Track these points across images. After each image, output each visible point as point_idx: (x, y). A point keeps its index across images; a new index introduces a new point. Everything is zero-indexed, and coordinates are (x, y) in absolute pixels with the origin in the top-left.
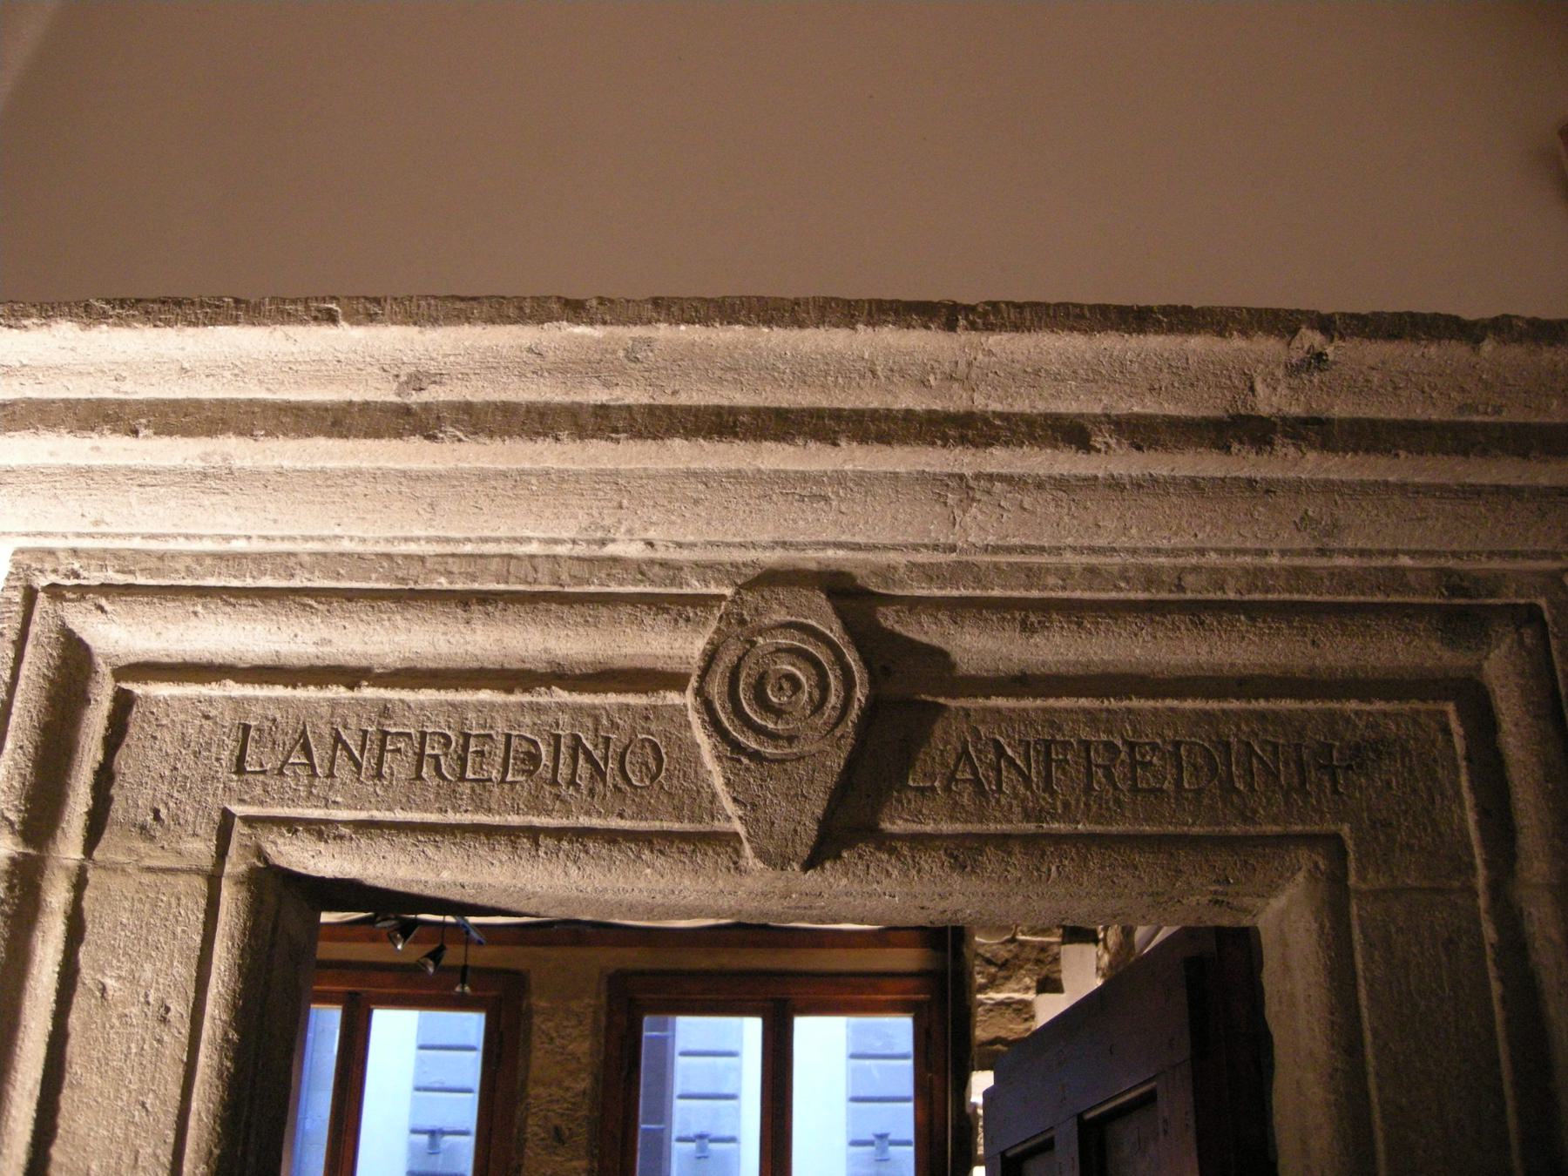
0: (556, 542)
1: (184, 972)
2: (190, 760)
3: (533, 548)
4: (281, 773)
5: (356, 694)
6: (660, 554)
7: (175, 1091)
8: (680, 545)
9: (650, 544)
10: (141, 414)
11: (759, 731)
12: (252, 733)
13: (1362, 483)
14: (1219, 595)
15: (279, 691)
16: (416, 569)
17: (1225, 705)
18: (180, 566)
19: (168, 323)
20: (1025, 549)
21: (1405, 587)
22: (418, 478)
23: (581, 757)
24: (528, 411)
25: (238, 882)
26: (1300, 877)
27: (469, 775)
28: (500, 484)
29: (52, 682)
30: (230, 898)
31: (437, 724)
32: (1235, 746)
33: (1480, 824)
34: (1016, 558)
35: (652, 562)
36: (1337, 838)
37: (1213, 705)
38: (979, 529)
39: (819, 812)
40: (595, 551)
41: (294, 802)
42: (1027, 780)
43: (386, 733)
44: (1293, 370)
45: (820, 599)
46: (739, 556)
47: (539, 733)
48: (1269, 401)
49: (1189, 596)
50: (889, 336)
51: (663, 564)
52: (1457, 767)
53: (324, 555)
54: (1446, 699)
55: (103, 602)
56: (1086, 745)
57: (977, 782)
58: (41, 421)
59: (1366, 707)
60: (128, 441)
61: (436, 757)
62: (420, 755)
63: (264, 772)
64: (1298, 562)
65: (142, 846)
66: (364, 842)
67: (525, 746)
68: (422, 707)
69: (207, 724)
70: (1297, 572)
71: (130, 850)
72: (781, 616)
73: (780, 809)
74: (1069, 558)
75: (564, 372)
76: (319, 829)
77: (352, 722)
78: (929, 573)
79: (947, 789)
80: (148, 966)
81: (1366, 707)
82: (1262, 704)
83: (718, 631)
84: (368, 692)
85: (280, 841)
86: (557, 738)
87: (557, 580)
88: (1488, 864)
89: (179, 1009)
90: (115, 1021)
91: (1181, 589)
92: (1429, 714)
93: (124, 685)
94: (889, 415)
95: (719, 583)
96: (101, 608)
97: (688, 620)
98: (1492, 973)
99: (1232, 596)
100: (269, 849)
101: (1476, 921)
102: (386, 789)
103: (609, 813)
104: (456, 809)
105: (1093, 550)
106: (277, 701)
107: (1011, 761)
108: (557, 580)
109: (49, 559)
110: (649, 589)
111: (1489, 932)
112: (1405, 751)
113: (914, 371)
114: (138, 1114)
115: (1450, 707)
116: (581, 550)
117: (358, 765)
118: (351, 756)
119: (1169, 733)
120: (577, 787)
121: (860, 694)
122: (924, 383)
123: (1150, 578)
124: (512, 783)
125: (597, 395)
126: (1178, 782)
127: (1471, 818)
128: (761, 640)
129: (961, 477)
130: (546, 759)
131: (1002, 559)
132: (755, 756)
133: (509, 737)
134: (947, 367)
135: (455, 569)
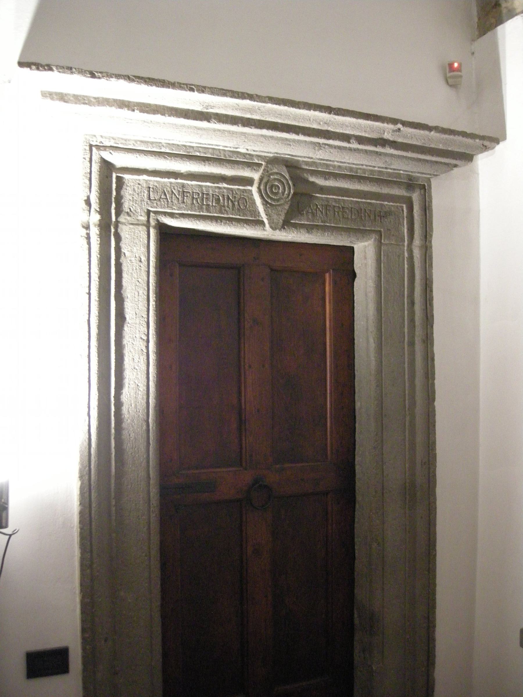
0: (226, 147)
1: (144, 250)
2: (137, 195)
3: (221, 148)
4: (160, 200)
5: (177, 181)
6: (249, 152)
7: (146, 278)
8: (254, 151)
9: (247, 150)
10: (134, 106)
11: (271, 199)
12: (151, 189)
13: (398, 155)
14: (364, 175)
15: (158, 179)
16: (191, 150)
17: (362, 200)
18: (131, 143)
19: (151, 85)
20: (327, 160)
21: (400, 178)
22: (199, 129)
23: (230, 202)
24: (232, 118)
25: (155, 227)
26: (373, 240)
27: (205, 203)
28: (218, 133)
29: (99, 172)
30: (152, 231)
31: (196, 190)
32: (363, 210)
33: (407, 232)
34: (325, 162)
35: (247, 154)
36: (380, 231)
37: (360, 200)
38: (319, 155)
39: (283, 218)
40: (235, 150)
41: (164, 208)
42: (322, 213)
43: (184, 192)
44: (394, 131)
45: (284, 168)
46: (266, 154)
47: (220, 194)
48: (386, 136)
49: (358, 174)
50: (317, 113)
51: (249, 154)
52: (404, 219)
53: (169, 144)
54: (404, 204)
55: (111, 151)
56: (334, 206)
57: (312, 213)
58: (107, 104)
59: (388, 204)
60: (130, 112)
61: (197, 198)
62: (193, 198)
63: (155, 200)
64: (380, 169)
65: (128, 218)
66: (182, 219)
67: (217, 197)
68: (192, 185)
69: (140, 186)
70: (380, 172)
71: (125, 219)
72: (275, 170)
73: (275, 217)
74: (336, 163)
75: (243, 110)
76: (172, 215)
77: (176, 188)
78: (307, 163)
79: (306, 214)
80: (135, 248)
81: (388, 204)
82: (369, 201)
83: (262, 173)
84: (179, 181)
85: (162, 218)
86: (224, 195)
87: (225, 156)
88: (408, 240)
89: (144, 259)
90: (129, 261)
91: (357, 173)
92: (400, 206)
93: (118, 175)
94: (309, 129)
95: (262, 161)
96: (111, 153)
97: (254, 169)
98: (406, 262)
99: (366, 176)
100: (159, 219)
101: (404, 252)
102: (186, 206)
103: (237, 215)
104: (203, 212)
105: (341, 162)
106: (157, 181)
107: (319, 209)
108: (225, 156)
109: (94, 138)
110: (246, 161)
111: (406, 255)
112: (395, 214)
113: (318, 120)
114: (138, 284)
115: (404, 206)
116: (232, 149)
117: (178, 199)
118: (176, 197)
119: (350, 205)
120: (229, 209)
121: (292, 192)
122: (320, 124)
123: (351, 169)
124: (215, 206)
125: (248, 116)
126: (351, 217)
127: (406, 231)
128: (272, 177)
129: (319, 143)
130: (221, 201)
131: (322, 162)
132: (270, 204)
133: (213, 194)
134: (325, 121)
135: (201, 151)
